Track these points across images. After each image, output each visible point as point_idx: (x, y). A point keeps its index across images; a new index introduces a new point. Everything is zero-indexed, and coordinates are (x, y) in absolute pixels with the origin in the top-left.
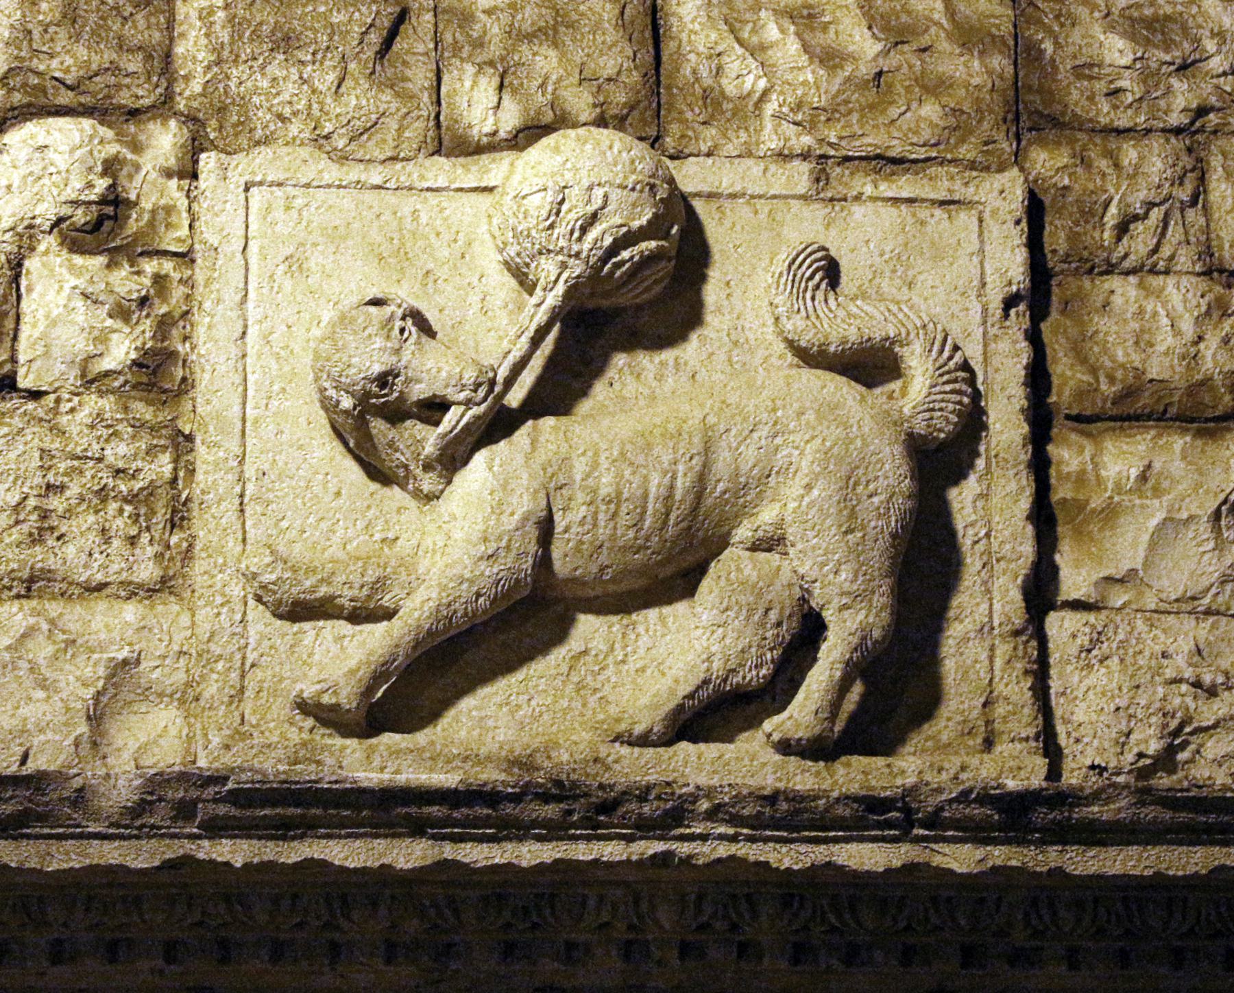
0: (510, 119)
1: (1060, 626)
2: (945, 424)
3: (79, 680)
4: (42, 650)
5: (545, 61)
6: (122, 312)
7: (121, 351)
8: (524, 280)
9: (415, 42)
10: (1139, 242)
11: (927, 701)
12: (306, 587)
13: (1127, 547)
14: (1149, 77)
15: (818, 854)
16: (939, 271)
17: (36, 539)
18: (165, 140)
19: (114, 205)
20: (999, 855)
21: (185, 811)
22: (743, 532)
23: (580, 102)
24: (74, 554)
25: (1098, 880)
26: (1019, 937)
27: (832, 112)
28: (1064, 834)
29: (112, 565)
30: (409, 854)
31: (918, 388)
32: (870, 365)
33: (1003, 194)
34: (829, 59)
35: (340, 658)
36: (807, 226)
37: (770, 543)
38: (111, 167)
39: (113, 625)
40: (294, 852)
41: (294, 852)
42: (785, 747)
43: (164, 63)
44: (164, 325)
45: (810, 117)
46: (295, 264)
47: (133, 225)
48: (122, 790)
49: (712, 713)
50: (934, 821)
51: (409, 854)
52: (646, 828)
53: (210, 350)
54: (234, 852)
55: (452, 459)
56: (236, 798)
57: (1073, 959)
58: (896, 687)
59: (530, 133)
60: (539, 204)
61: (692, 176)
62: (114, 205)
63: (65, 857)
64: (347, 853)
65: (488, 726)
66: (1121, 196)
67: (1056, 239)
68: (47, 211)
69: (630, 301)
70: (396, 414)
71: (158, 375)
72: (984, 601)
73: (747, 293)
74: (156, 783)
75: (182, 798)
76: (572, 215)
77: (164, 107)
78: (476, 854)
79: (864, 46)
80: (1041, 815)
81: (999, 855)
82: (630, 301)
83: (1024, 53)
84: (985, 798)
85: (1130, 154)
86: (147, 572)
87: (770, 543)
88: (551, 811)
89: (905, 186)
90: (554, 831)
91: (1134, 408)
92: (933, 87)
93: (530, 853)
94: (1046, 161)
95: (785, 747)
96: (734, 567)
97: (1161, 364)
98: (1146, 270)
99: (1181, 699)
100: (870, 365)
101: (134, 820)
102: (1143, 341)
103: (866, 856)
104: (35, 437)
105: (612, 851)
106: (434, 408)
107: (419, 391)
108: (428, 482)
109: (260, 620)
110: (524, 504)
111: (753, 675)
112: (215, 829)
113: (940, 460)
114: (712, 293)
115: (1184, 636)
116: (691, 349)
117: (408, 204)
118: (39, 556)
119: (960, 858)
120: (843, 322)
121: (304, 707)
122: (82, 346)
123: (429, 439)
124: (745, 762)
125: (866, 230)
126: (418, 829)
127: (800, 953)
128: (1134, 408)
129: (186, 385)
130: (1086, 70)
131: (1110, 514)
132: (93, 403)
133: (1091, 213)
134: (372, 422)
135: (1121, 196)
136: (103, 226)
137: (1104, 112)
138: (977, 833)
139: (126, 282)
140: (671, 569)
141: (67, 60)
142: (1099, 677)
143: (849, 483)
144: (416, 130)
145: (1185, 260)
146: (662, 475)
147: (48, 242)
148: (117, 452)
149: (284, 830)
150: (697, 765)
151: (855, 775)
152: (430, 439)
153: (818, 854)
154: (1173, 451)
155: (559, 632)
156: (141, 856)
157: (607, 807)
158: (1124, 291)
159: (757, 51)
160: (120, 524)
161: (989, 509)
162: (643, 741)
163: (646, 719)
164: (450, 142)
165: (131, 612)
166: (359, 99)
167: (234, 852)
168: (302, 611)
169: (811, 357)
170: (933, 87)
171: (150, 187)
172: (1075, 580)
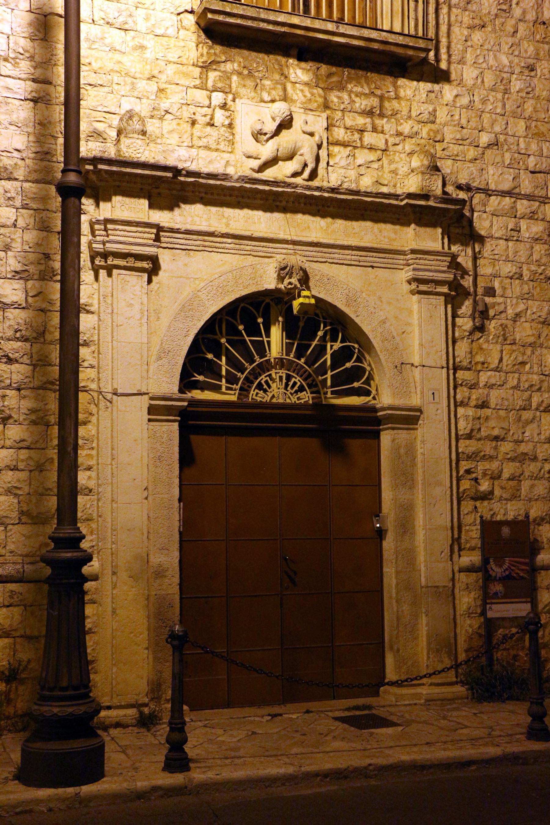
0: (269, 99)
1: (329, 168)
2: (320, 143)
3: (223, 162)
4: (219, 158)
5: (274, 92)
6: (227, 118)
7: (227, 122)
8: (274, 119)
9: (258, 88)
10: (338, 124)
11: (316, 176)
12: (250, 154)
13: (337, 159)
14: (339, 103)
15: (311, 193)
16: (318, 123)
17: (218, 144)
18: (230, 97)
19: (225, 104)
20: (330, 195)
21: (243, 180)
22: (299, 153)
23: (277, 98)
24: (222, 147)
25: (340, 199)
26: (329, 204)
27: (305, 103)
28: (337, 193)
29: (225, 149)
30: (267, 188)
31: (317, 138)
32: (312, 134)
33: (324, 115)
34: (305, 96)
35: (256, 164)
36: (304, 117)
37: (301, 155)
38: (225, 99)
39: (226, 156)
40: (254, 186)
41: (254, 186)
42: (304, 180)
43: (230, 87)
44: (232, 120)
45: (302, 103)
46: (247, 114)
47: (227, 107)
48: (236, 177)
49: (295, 175)
50: (324, 190)
51: (267, 188)
52: (293, 188)
53: (237, 123)
54: (248, 186)
55: (267, 140)
56: (249, 179)
57: (334, 207)
58: (313, 175)
59: (273, 101)
60: (277, 111)
61: (293, 109)
62: (225, 104)
63: (229, 184)
64: (261, 187)
65: (269, 174)
66: (337, 118)
67: (329, 122)
68: (218, 104)
69: (286, 124)
70: (261, 134)
71: (230, 126)
72: (322, 165)
73: (297, 123)
74: (240, 176)
75: (242, 179)
76: (281, 112)
77: (230, 92)
78: (275, 189)
79: (309, 95)
80: (336, 191)
81: (330, 195)
82: (286, 124)
83: (325, 99)
84: (330, 188)
85: (337, 112)
86: (230, 150)
87: (301, 155)
88: (283, 185)
89: (314, 113)
90: (283, 187)
91: (337, 143)
92: (316, 101)
93: (280, 189)
94: (328, 112)
95: (304, 180)
96: (297, 158)
97: (341, 138)
98: (339, 127)
99: (343, 178)
100: (312, 134)
101: (237, 181)
102: (338, 135)
103: (316, 193)
104: (217, 132)
105: (289, 190)
106: (265, 134)
107: (264, 132)
108: (264, 143)
109: (244, 158)
110: (276, 147)
111: (300, 170)
112: (246, 183)
113: (319, 147)
114: (293, 123)
115: (343, 171)
116: (291, 130)
117: (260, 108)
118: (218, 147)
119: (326, 195)
120: (309, 129)
121: (251, 169)
122: (222, 121)
123: (265, 138)
124: (298, 180)
125: (310, 118)
126: (268, 185)
127: (305, 204)
128: (337, 143)
129: (234, 128)
130: (332, 102)
131: (335, 155)
132: (223, 129)
133: (333, 119)
134: (258, 135)
135: (337, 118)
136: (224, 106)
137: (334, 107)
138: (328, 192)
139: (227, 113)
140: (290, 158)
141: (220, 85)
142: (334, 175)
143: (312, 148)
144: (259, 99)
145: (343, 126)
146: (291, 146)
147: (218, 108)
148: (227, 135)
149: (254, 184)
150: (293, 180)
151: (310, 183)
152: (265, 138)
153: (311, 193)
154: (342, 148)
155: (277, 163)
156: (238, 185)
157: (289, 185)
158: (336, 129)
159: (297, 94)
160: (227, 144)
161: (323, 153)
162: (288, 177)
163: (289, 175)
164: (262, 101)
165: (228, 155)
166: (253, 94)
167: (248, 186)
168: (249, 157)
169: (304, 133)
170: (316, 101)
171: (230, 103)
172: (331, 164)
